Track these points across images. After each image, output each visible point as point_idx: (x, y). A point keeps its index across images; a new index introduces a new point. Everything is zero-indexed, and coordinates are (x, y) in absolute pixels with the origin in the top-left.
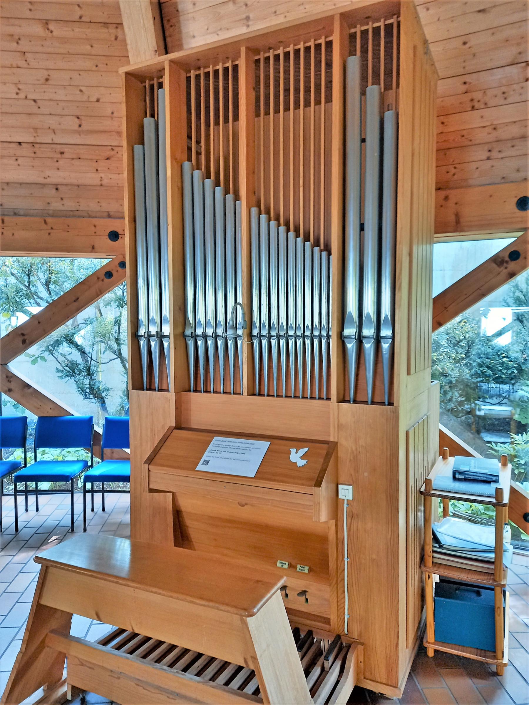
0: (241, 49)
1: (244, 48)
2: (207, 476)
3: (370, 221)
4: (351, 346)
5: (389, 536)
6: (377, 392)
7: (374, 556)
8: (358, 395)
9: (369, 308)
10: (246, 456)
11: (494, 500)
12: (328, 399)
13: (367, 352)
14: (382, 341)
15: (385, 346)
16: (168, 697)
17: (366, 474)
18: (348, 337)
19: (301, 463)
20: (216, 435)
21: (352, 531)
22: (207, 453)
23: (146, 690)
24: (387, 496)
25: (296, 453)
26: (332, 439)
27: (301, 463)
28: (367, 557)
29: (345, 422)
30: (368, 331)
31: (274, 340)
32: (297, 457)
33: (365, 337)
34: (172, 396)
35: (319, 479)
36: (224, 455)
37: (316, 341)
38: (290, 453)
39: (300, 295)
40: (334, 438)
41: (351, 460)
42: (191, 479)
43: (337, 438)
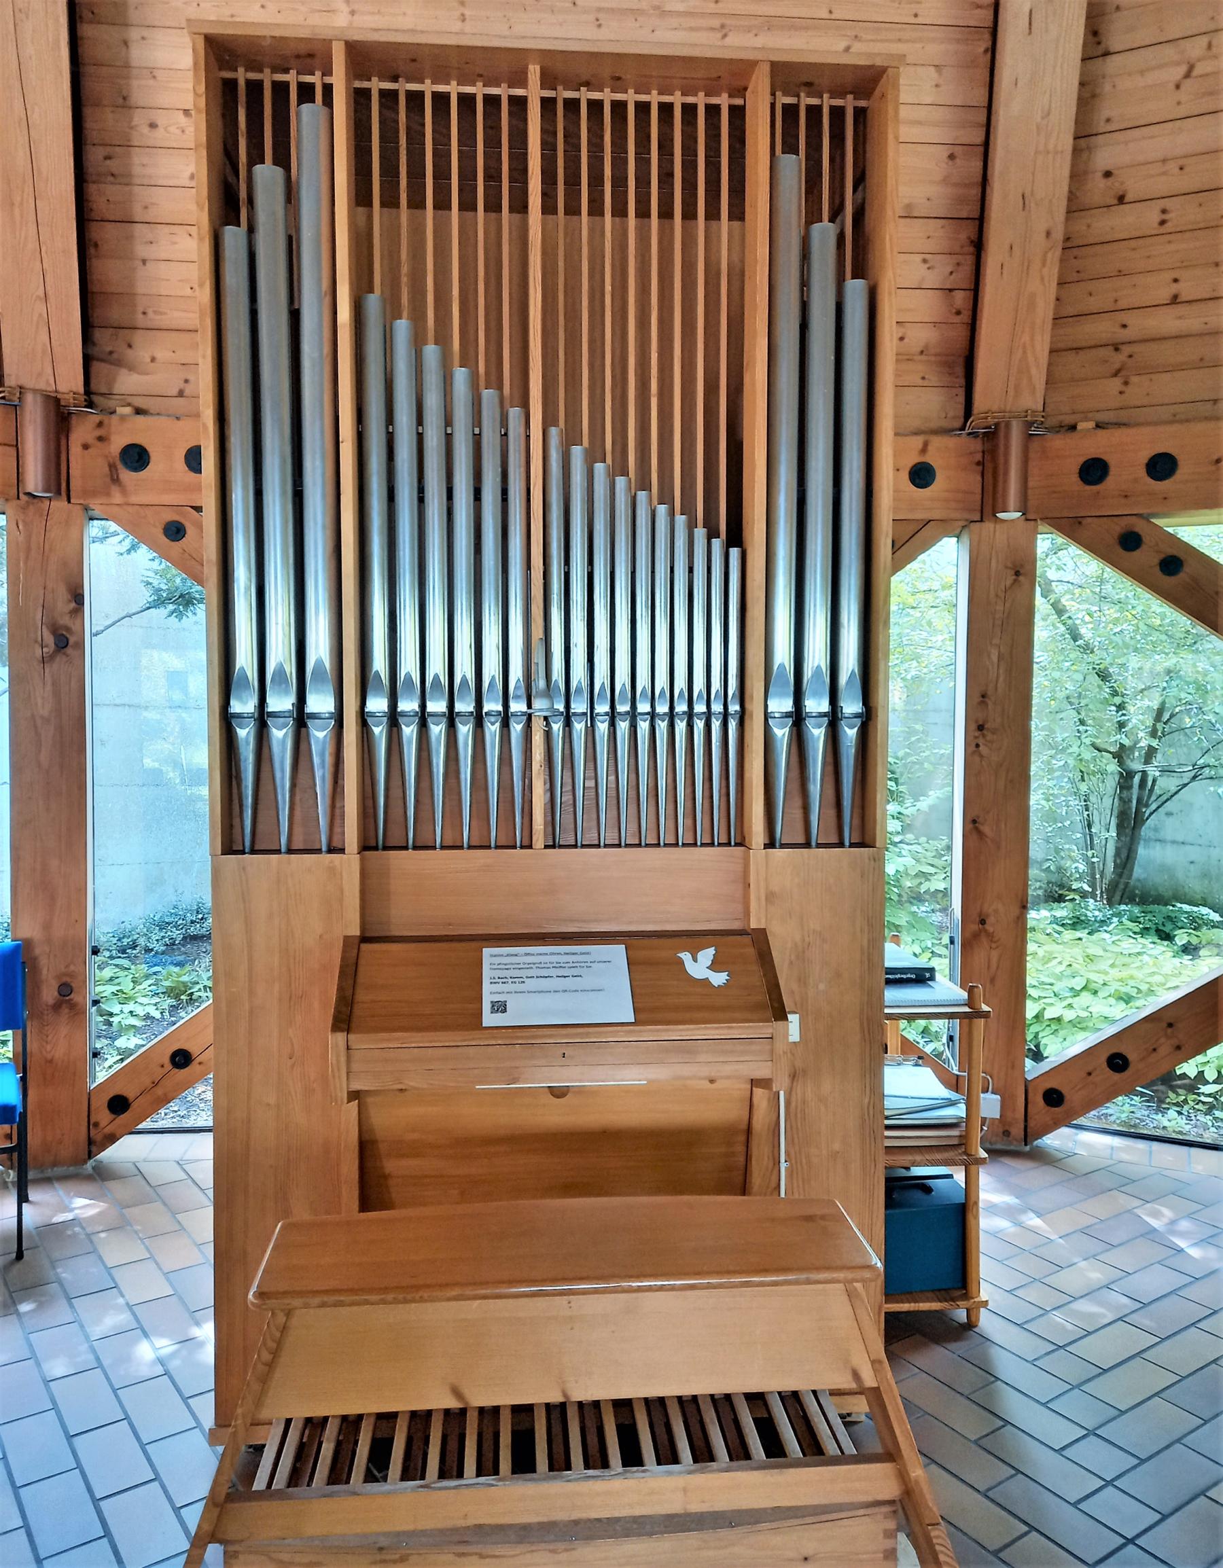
0: (531, 67)
1: (538, 68)
2: (518, 1038)
3: (406, 465)
4: (245, 733)
5: (867, 1101)
6: (298, 830)
7: (837, 1146)
8: (257, 841)
9: (280, 652)
10: (587, 981)
11: (967, 1009)
12: (335, 849)
13: (276, 749)
14: (310, 723)
15: (850, 733)
16: (552, 1551)
17: (822, 987)
18: (239, 716)
19: (719, 979)
20: (484, 943)
21: (793, 1104)
22: (487, 987)
23: (488, 1557)
24: (862, 1024)
25: (695, 960)
26: (753, 925)
27: (719, 979)
28: (824, 1152)
29: (787, 886)
30: (281, 702)
31: (603, 722)
32: (699, 965)
33: (273, 715)
34: (350, 862)
35: (776, 1005)
36: (531, 984)
37: (699, 725)
38: (681, 963)
39: (645, 626)
40: (759, 920)
41: (791, 963)
42: (471, 1050)
43: (763, 921)
